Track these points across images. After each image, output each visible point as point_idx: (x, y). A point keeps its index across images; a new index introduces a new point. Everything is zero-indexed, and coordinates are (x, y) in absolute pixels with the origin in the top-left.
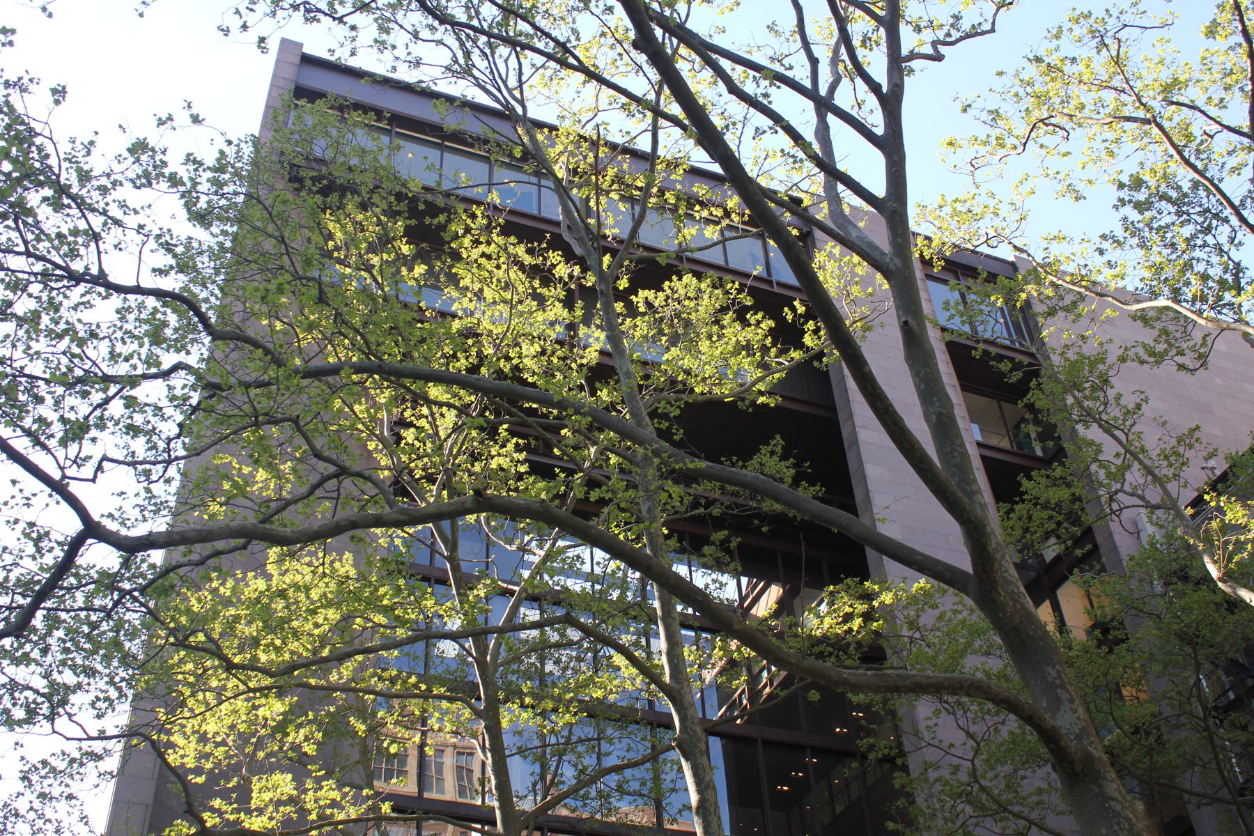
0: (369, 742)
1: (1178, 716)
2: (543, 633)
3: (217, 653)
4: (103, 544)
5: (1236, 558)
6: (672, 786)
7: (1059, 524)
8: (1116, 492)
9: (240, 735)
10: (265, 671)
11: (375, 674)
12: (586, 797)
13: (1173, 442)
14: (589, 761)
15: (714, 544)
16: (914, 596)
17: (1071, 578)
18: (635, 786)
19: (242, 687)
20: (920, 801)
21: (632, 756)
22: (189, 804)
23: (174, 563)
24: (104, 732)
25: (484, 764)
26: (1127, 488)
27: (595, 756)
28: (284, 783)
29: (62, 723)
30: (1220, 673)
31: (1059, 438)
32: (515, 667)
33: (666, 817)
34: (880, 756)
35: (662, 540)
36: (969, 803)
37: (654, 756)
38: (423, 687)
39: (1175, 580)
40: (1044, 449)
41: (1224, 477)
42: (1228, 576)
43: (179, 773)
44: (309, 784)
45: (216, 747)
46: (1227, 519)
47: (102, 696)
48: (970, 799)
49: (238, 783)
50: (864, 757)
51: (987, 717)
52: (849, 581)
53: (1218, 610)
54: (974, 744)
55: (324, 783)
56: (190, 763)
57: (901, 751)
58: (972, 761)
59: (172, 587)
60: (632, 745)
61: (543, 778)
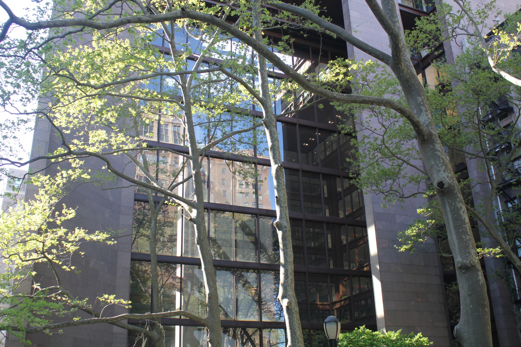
0: (137, 119)
1: (468, 123)
2: (210, 76)
3: (73, 80)
4: (22, 27)
5: (502, 58)
6: (261, 140)
7: (430, 40)
8: (456, 28)
9: (84, 114)
10: (95, 87)
11: (139, 91)
12: (225, 144)
13: (483, 7)
14: (228, 129)
15: (283, 41)
16: (366, 67)
17: (432, 64)
18: (246, 140)
19: (84, 94)
20: (360, 151)
21: (246, 128)
22: (64, 141)
23: (51, 37)
24: (26, 111)
25: (184, 129)
26: (460, 26)
27: (230, 127)
28: (102, 134)
29: (8, 107)
30: (487, 107)
31: (434, 3)
32: (198, 90)
33: (258, 152)
34: (346, 132)
35: (261, 37)
36: (380, 153)
37: (254, 129)
38: (160, 96)
39: (475, 67)
40: (427, 8)
41: (502, 25)
42: (497, 66)
43: (59, 129)
44: (113, 135)
45: (74, 119)
46: (501, 41)
47: (24, 97)
48: (380, 150)
49: (84, 134)
50: (340, 133)
51: (391, 119)
52: (339, 59)
53: (490, 81)
54: (385, 130)
55: (119, 134)
56: (64, 125)
57: (355, 130)
58: (383, 136)
59: (51, 47)
60: (246, 124)
61: (208, 136)
